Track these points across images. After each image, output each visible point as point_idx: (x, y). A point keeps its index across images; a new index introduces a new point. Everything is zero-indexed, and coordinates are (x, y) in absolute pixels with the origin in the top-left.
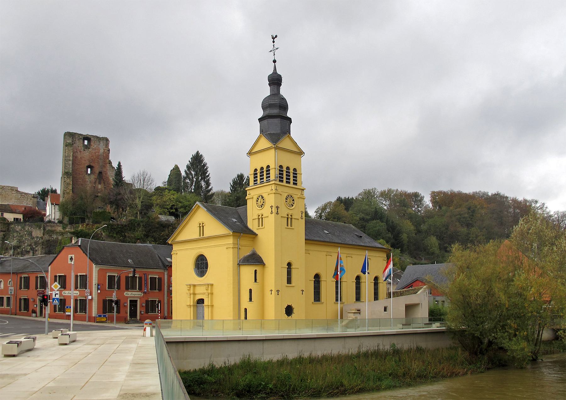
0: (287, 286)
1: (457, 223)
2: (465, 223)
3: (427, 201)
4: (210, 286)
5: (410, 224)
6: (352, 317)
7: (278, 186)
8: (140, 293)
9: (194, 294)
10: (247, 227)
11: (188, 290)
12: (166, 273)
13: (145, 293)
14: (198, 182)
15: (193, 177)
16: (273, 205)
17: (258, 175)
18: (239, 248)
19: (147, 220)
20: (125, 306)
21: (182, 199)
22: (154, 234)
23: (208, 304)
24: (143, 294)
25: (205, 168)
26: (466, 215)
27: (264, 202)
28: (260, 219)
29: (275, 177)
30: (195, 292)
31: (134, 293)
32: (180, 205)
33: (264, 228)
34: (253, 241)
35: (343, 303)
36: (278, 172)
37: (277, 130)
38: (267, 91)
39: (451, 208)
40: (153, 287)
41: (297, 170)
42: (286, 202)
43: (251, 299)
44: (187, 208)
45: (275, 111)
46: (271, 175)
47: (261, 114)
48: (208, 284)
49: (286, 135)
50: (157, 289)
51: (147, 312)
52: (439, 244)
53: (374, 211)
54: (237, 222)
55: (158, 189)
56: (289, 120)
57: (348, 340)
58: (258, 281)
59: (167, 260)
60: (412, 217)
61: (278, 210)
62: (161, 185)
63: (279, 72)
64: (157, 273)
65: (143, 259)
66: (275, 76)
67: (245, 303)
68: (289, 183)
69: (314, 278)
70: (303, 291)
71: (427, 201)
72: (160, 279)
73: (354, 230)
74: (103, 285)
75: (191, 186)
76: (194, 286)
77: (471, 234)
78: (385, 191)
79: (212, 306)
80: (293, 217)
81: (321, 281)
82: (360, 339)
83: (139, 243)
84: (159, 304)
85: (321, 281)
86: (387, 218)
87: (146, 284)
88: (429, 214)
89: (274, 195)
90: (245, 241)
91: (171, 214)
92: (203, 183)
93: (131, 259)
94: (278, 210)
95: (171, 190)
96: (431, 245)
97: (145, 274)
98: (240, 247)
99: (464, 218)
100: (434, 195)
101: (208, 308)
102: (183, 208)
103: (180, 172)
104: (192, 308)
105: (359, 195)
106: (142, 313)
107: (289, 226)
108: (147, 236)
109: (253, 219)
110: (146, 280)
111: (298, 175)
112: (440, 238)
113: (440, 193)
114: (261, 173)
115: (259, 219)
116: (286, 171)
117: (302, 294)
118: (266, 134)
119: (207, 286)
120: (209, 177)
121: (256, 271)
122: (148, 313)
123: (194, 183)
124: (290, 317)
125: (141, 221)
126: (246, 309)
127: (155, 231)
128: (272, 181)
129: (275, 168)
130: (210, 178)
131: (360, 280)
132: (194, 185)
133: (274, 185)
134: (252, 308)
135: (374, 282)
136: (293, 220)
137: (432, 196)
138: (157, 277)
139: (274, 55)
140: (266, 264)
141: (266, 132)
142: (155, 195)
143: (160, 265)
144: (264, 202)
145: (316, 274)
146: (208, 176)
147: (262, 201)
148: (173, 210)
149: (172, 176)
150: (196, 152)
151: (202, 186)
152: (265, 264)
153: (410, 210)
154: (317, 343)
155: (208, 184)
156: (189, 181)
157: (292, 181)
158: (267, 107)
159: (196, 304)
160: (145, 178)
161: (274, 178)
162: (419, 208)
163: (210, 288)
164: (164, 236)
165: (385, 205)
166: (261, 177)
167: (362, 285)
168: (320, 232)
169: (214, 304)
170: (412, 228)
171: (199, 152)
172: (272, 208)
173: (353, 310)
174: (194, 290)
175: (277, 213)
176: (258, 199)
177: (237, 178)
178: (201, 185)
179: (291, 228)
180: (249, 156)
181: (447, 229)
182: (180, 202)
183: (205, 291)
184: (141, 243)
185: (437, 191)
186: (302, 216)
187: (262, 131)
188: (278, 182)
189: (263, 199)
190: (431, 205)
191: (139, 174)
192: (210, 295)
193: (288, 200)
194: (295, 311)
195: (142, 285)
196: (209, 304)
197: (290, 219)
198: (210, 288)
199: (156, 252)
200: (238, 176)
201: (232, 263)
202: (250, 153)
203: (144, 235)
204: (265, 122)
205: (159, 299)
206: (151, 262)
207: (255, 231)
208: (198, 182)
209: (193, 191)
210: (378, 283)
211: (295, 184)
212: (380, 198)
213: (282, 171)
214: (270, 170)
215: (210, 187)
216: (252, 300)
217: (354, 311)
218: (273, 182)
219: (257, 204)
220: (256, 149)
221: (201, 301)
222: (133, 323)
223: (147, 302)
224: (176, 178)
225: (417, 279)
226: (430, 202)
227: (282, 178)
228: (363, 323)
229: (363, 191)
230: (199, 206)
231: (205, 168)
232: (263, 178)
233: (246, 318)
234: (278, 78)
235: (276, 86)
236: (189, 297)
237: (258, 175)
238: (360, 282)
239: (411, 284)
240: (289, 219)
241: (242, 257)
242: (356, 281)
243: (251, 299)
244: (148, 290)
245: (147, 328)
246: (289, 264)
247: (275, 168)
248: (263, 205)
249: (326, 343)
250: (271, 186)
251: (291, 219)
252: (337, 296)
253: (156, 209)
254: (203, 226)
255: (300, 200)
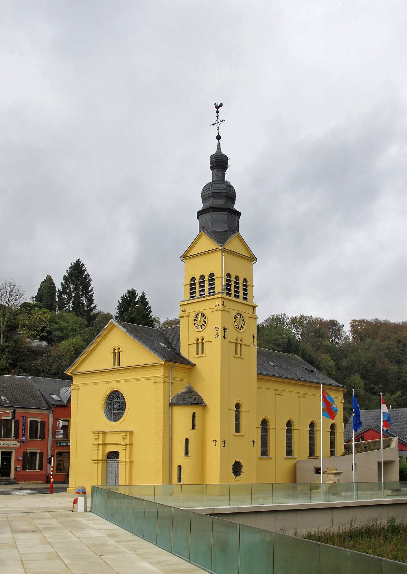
0: (235, 435)
1: (386, 359)
2: (394, 359)
3: (347, 330)
4: (128, 434)
5: (329, 358)
6: (333, 480)
7: (226, 301)
8: (16, 442)
9: (104, 445)
10: (179, 355)
11: (95, 439)
12: (51, 415)
13: (22, 442)
14: (78, 298)
15: (71, 292)
16: (219, 326)
17: (197, 286)
18: (172, 383)
19: (13, 345)
20: (19, 460)
21: (58, 319)
22: (23, 363)
23: (126, 458)
24: (19, 444)
25: (87, 281)
26: (397, 350)
27: (205, 322)
28: (200, 345)
29: (222, 289)
30: (105, 441)
31: (7, 442)
32: (56, 326)
33: (205, 356)
34: (189, 373)
35: (271, 459)
36: (225, 282)
37: (224, 228)
38: (208, 177)
39: (377, 341)
40: (33, 434)
41: (248, 280)
42: (235, 322)
43: (187, 453)
44: (64, 331)
45: (220, 203)
46: (215, 286)
47: (200, 206)
48: (126, 431)
49: (235, 234)
50: (38, 437)
51: (24, 468)
52: (365, 384)
53: (287, 341)
54: (166, 348)
55: (25, 305)
56: (238, 215)
57: (336, 513)
58: (196, 428)
59: (52, 398)
60: (330, 350)
61: (225, 333)
62: (29, 301)
63: (224, 151)
64: (38, 415)
65: (20, 396)
66: (219, 156)
67: (179, 457)
68: (237, 297)
69: (309, 428)
70: (254, 442)
71: (347, 330)
72: (43, 423)
73: (302, 362)
74: (181, 440)
75: (69, 303)
76: (105, 433)
77: (403, 373)
78: (296, 318)
79: (131, 462)
80: (243, 343)
81: (269, 428)
82: (351, 511)
83: (14, 374)
84: (52, 458)
85: (269, 428)
86: (304, 351)
87: (25, 430)
88: (348, 347)
89: (220, 312)
90: (179, 373)
91: (42, 338)
92: (84, 299)
93: (5, 395)
94: (225, 333)
95: (42, 308)
96: (354, 385)
97: (23, 416)
98: (173, 381)
99: (394, 353)
100: (355, 324)
101: (126, 464)
102: (59, 330)
103: (53, 284)
104: (100, 464)
105: (266, 321)
106: (18, 469)
107: (239, 355)
108: (13, 366)
109: (211, 341)
110: (25, 425)
111: (249, 288)
112: (365, 377)
113: (362, 322)
114: (201, 283)
115: (198, 344)
116: (235, 282)
117: (253, 446)
118: (208, 232)
119: (125, 434)
120: (92, 293)
121: (194, 414)
122: (25, 470)
123: (73, 299)
124: (238, 477)
125: (6, 346)
126: (180, 467)
127: (24, 360)
128: (217, 294)
129: (221, 277)
130: (93, 293)
131: (314, 428)
132: (72, 301)
133: (220, 299)
134: (187, 464)
135: (330, 430)
136: (243, 346)
137: (352, 326)
138: (39, 420)
139: (218, 129)
140: (207, 405)
141: (207, 230)
142: (21, 313)
143: (43, 405)
144: (205, 322)
145: (263, 419)
146: (91, 291)
147: (203, 320)
148: (43, 334)
149: (42, 290)
150: (76, 261)
151: (83, 304)
152: (206, 405)
153: (327, 341)
154: (300, 518)
155: (91, 300)
156: (66, 297)
157: (241, 295)
158: (209, 197)
159: (106, 459)
160: (12, 289)
161: (220, 291)
162: (337, 340)
163: (128, 437)
164: (37, 366)
165: (298, 333)
166: (200, 288)
167: (317, 434)
168: (266, 364)
169: (133, 459)
170: (332, 363)
171: (80, 260)
172: (217, 330)
173: (333, 469)
174: (104, 439)
175: (224, 337)
176: (196, 317)
177: (127, 295)
178: (82, 303)
179: (241, 357)
180: (183, 260)
181: (373, 366)
182: (56, 323)
183: (121, 441)
184: (15, 374)
185: (359, 319)
186: (253, 342)
187: (202, 228)
188: (225, 296)
189: (204, 318)
190: (351, 336)
191: (4, 285)
192: (128, 446)
193: (237, 320)
194: (244, 469)
195: (18, 429)
196: (127, 459)
197: (239, 345)
198: (128, 437)
199: (36, 386)
200: (129, 292)
201: (162, 402)
202: (185, 257)
203: (9, 365)
204: (207, 216)
205: (40, 450)
206: (32, 400)
207: (192, 360)
208: (78, 298)
209: (71, 309)
210: (335, 432)
211: (245, 299)
212: (291, 326)
213: (230, 281)
214: (214, 279)
215: (93, 305)
216: (188, 454)
217: (334, 471)
218: (220, 295)
219: (195, 323)
220: (193, 252)
221: (114, 455)
222: (6, 484)
223: (25, 454)
224: (48, 292)
225: (370, 428)
226: (349, 333)
227: (230, 290)
228: (348, 486)
229: (271, 317)
230: (114, 325)
231: (87, 281)
232: (195, 292)
233: (180, 479)
234: (223, 159)
235: (221, 169)
236: (97, 448)
237: (197, 286)
238: (314, 431)
239: (362, 433)
240: (238, 344)
241: (174, 395)
242: (309, 429)
243: (187, 453)
244: (26, 439)
245: (79, 498)
246: (238, 406)
247: (221, 277)
248: (204, 326)
249: (310, 517)
250: (216, 300)
251: (241, 344)
252: (311, 442)
253: (22, 332)
254: (120, 352)
255: (251, 320)
